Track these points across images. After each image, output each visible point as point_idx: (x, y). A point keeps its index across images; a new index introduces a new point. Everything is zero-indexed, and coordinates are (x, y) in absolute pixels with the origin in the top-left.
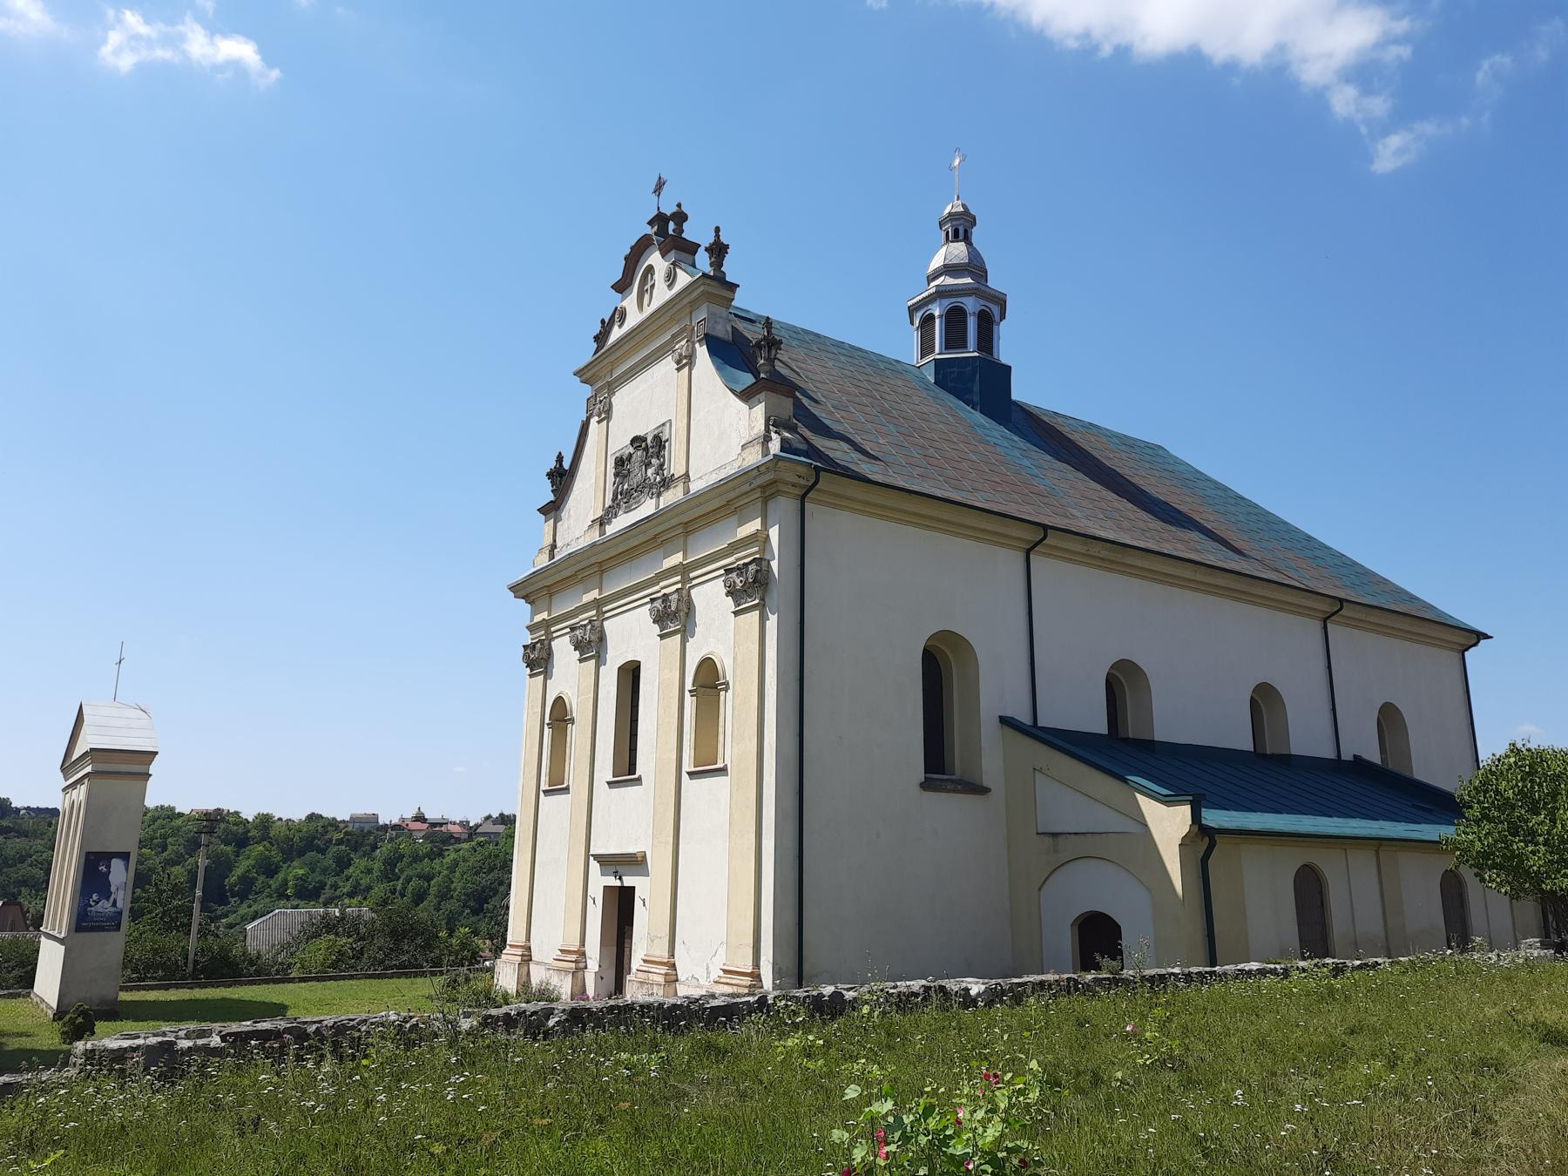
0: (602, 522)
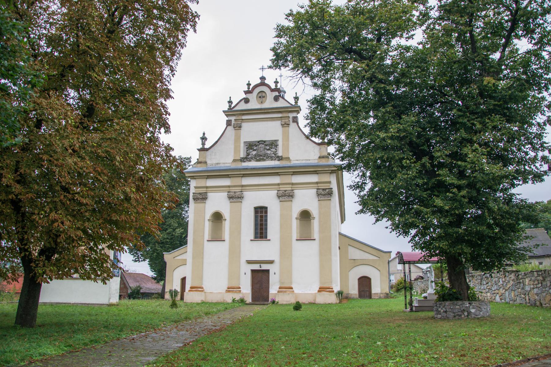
0: (243, 160)
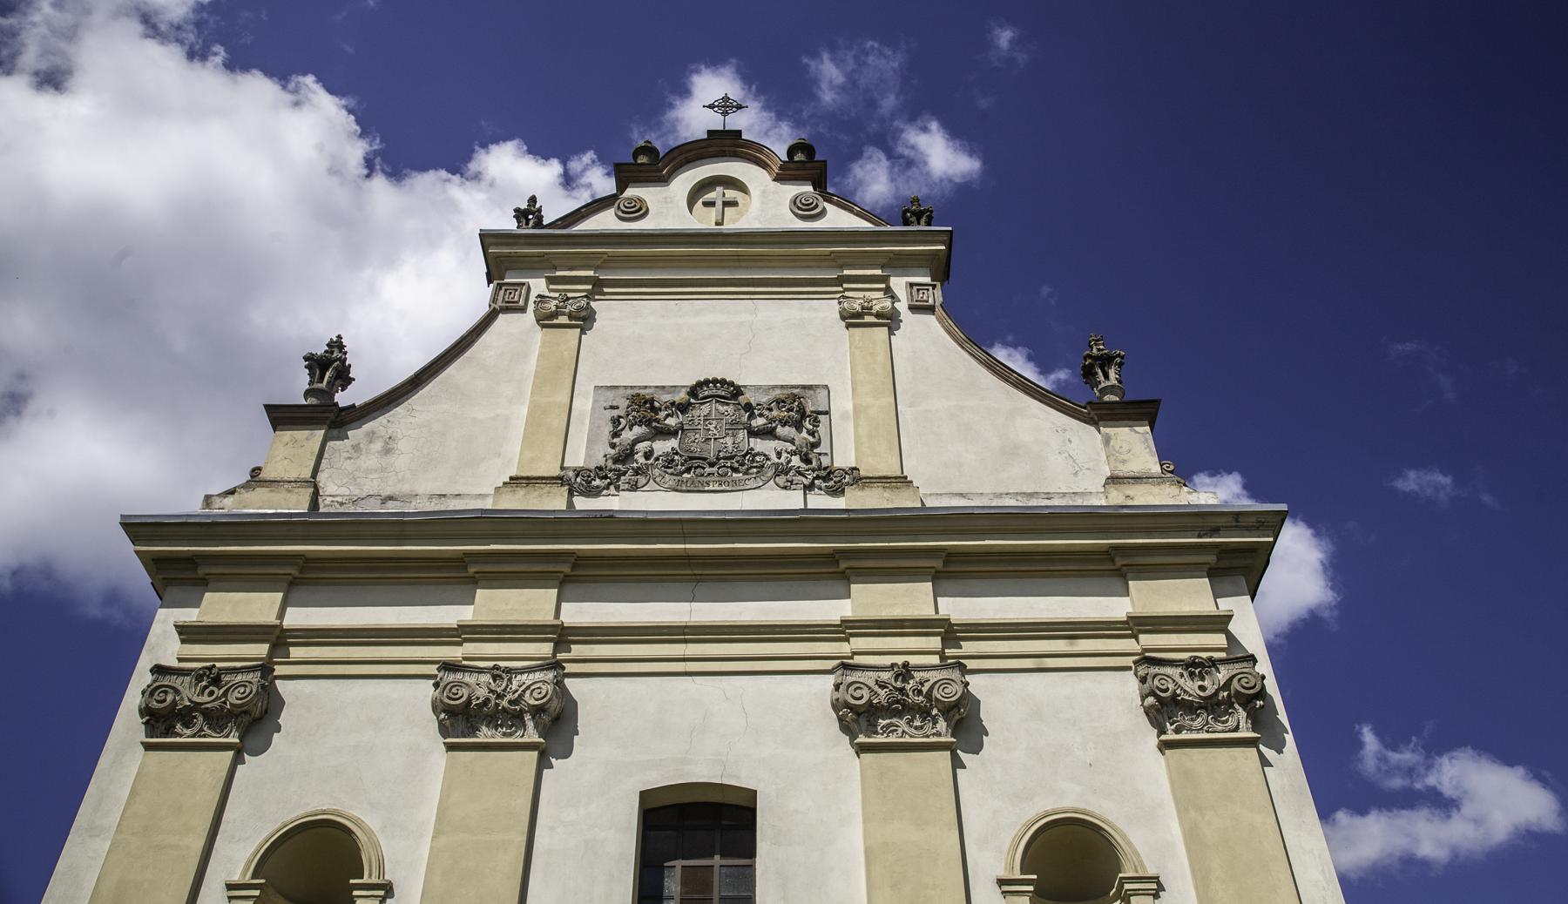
0: (583, 482)
